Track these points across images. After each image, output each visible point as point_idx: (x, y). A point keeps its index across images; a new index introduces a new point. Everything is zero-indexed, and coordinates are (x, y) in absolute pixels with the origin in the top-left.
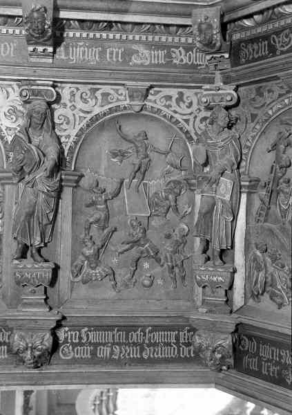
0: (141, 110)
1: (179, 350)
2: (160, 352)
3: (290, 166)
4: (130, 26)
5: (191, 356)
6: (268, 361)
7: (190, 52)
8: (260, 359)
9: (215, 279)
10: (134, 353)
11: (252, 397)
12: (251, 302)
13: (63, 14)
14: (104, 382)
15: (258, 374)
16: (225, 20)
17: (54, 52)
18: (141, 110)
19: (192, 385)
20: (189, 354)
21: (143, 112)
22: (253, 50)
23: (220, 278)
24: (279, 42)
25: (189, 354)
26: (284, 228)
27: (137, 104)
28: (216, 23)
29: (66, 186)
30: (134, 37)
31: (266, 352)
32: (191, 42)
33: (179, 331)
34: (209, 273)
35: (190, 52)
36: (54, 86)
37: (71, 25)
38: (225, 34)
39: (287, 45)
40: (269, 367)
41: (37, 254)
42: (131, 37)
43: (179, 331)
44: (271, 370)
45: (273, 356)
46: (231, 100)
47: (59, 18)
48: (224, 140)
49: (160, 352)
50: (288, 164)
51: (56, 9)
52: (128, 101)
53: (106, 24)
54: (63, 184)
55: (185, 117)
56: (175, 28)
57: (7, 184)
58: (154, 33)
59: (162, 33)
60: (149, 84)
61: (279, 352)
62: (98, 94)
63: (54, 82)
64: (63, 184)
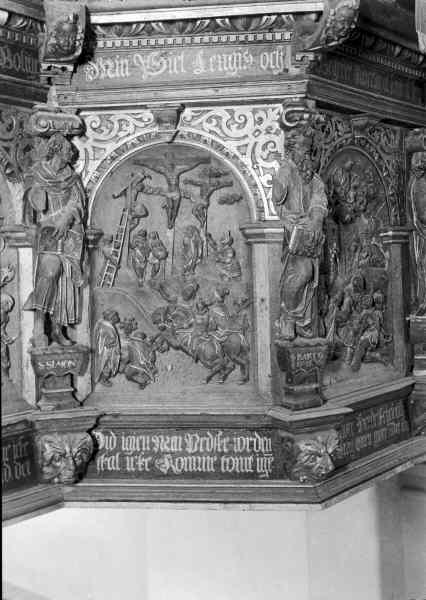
1: (13, 472)
3: (147, 215)
6: (135, 453)
7: (18, 54)
8: (123, 456)
9: (63, 364)
12: (99, 387)
13: (95, 19)
14: (97, 499)
15: (124, 474)
17: (75, 71)
19: (41, 511)
20: (26, 472)
22: (107, 67)
23: (70, 362)
24: (146, 64)
26: (143, 292)
29: (256, 242)
31: (131, 443)
33: (12, 444)
34: (56, 357)
35: (18, 54)
36: (77, 113)
39: (158, 70)
40: (136, 461)
41: (62, 336)
43: (12, 444)
44: (140, 463)
45: (141, 446)
48: (68, 179)
50: (144, 213)
51: (88, 14)
55: (5, 144)
57: (21, 247)
61: (151, 439)
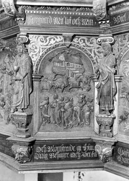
0: (70, 46)
2: (44, 156)
4: (35, 7)
5: (89, 157)
10: (45, 157)
11: (126, 175)
16: (109, 4)
18: (70, 46)
20: (89, 156)
21: (70, 47)
25: (89, 156)
27: (68, 43)
28: (105, 7)
29: (35, 81)
30: (45, 12)
32: (62, 14)
37: (86, 10)
38: (108, 11)
42: (35, 12)
46: (100, 42)
47: (17, 5)
49: (44, 156)
52: (64, 42)
53: (44, 7)
54: (33, 80)
56: (75, 8)
58: (85, 11)
59: (88, 11)
60: (73, 34)
62: (48, 39)
63: (27, 33)
64: (33, 80)
